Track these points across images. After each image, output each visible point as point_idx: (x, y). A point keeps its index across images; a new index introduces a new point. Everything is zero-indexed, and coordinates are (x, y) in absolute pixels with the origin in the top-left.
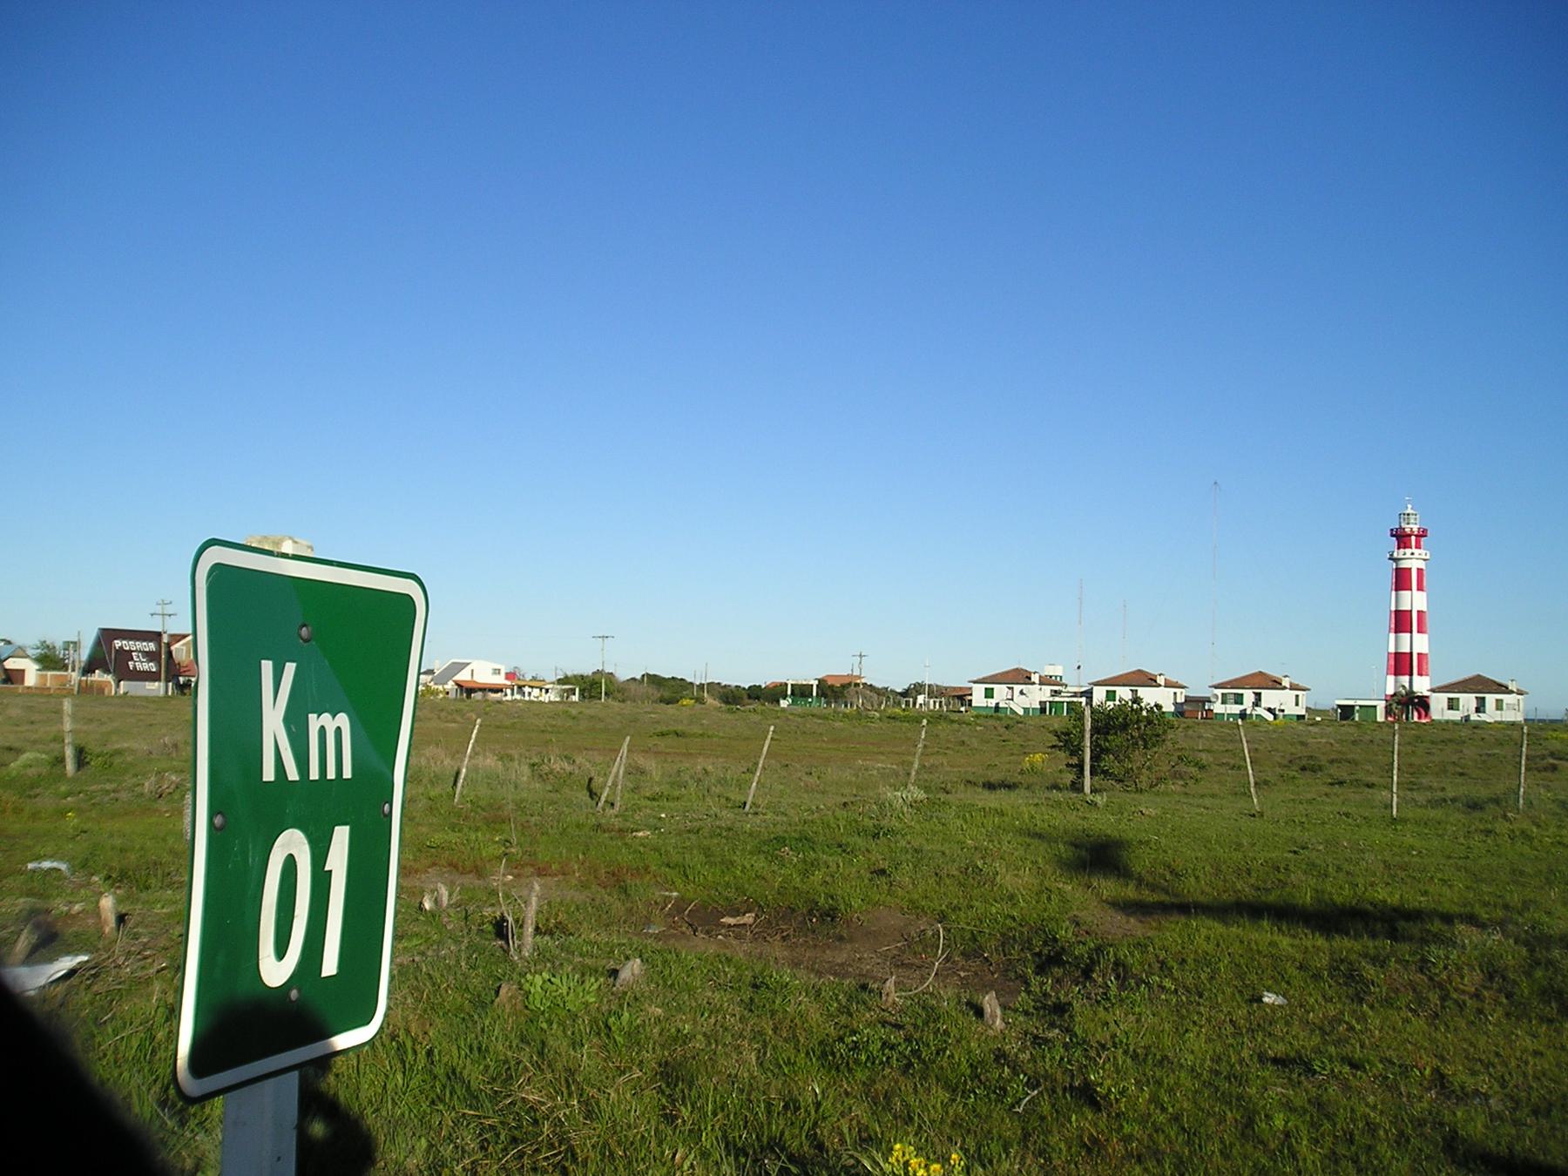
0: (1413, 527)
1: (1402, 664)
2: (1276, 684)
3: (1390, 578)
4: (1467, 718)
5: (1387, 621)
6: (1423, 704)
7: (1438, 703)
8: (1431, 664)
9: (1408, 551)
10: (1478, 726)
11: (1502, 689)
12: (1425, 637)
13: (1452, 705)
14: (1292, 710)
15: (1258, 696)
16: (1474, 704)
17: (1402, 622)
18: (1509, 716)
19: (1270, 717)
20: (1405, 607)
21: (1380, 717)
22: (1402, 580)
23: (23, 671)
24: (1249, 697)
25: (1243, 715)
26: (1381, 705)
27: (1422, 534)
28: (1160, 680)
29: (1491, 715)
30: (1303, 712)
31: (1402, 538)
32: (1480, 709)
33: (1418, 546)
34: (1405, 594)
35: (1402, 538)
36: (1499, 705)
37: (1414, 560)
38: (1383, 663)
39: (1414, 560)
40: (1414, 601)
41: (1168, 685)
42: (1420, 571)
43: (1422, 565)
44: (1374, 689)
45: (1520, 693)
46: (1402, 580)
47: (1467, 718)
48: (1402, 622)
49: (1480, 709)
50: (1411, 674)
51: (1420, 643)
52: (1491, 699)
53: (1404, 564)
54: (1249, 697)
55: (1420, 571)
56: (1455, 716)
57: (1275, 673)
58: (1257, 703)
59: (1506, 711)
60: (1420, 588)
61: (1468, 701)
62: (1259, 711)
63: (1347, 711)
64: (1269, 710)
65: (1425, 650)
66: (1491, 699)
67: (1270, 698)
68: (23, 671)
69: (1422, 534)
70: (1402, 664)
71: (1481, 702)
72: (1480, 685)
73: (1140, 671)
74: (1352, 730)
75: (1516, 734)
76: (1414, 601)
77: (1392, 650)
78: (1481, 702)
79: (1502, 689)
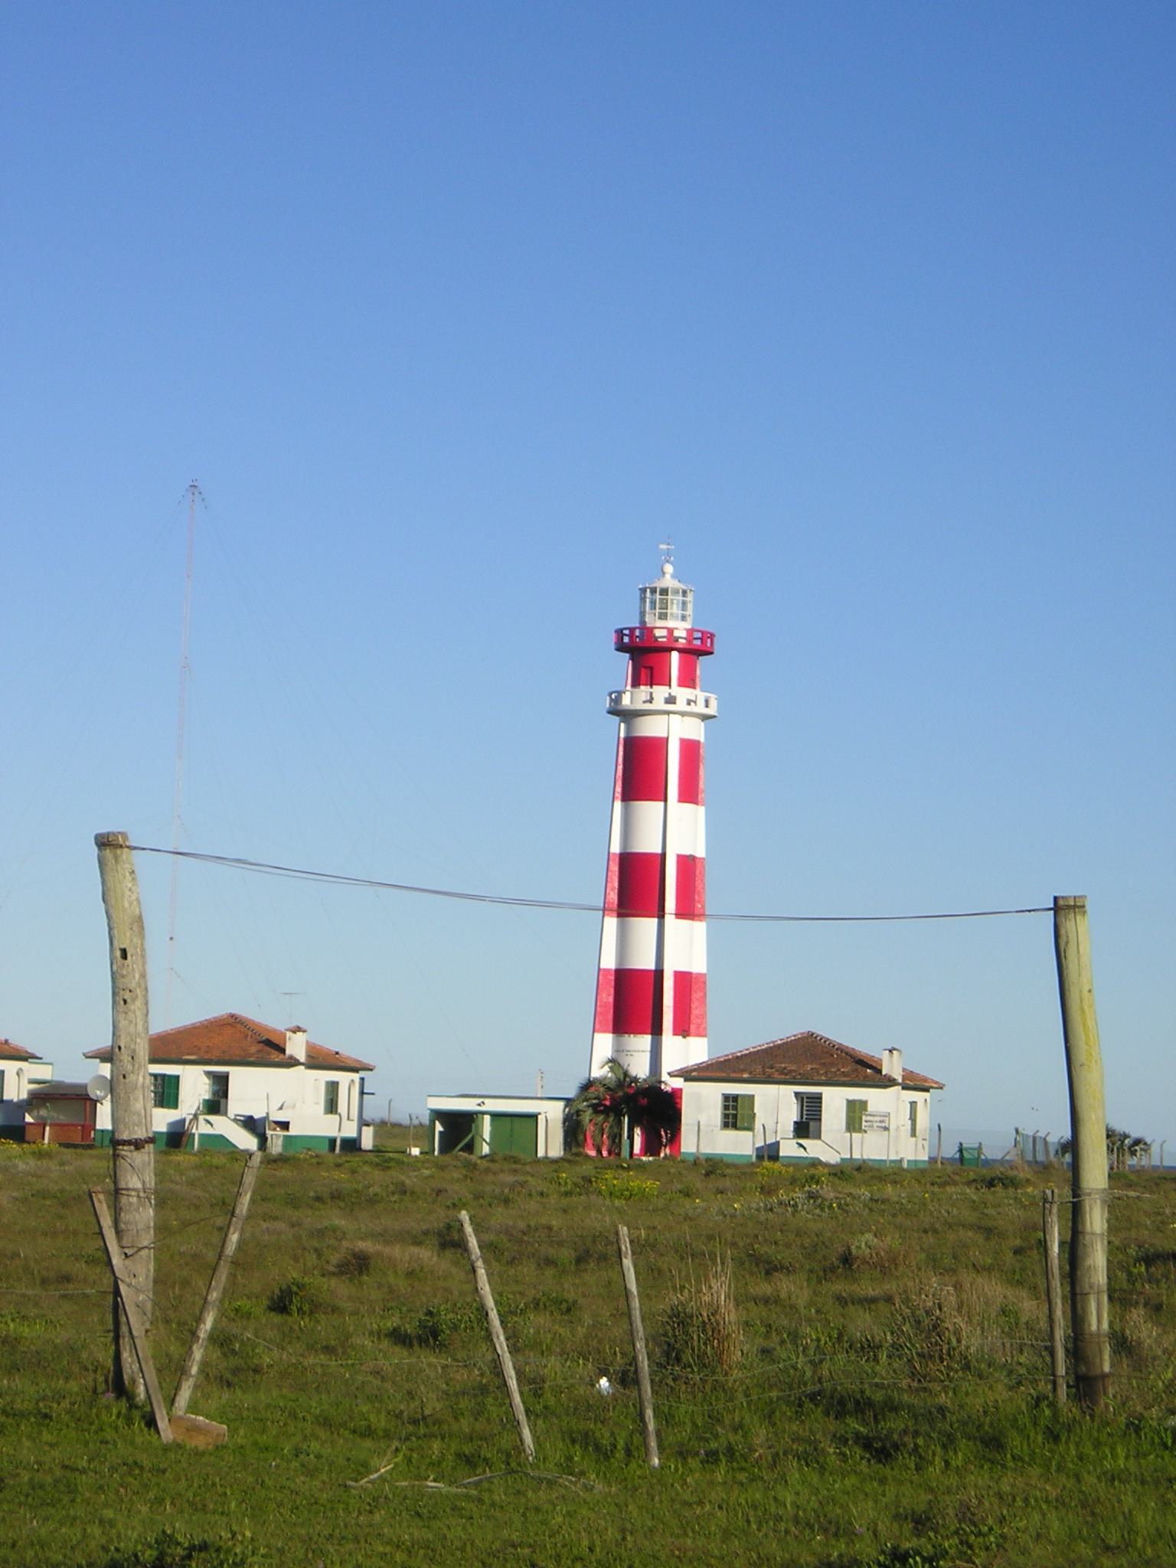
0: (676, 625)
1: (633, 1002)
2: (268, 1050)
3: (607, 765)
4: (770, 1152)
5: (599, 883)
6: (654, 1109)
7: (702, 1106)
8: (714, 1006)
9: (660, 692)
10: (809, 1172)
11: (863, 1071)
12: (699, 928)
13: (736, 1114)
14: (310, 1120)
15: (221, 1083)
16: (791, 1113)
17: (637, 886)
18: (871, 1148)
19: (247, 1141)
20: (648, 844)
21: (550, 1143)
22: (640, 772)
23: (178, 1077)
24: (195, 1084)
25: (177, 1137)
26: (552, 1113)
27: (697, 650)
28: (296, 1046)
29: (832, 1145)
30: (350, 1131)
31: (645, 656)
32: (807, 1126)
33: (688, 680)
34: (649, 811)
35: (645, 656)
36: (855, 1114)
37: (675, 717)
38: (585, 999)
39: (675, 717)
40: (675, 829)
41: (319, 1060)
42: (690, 749)
43: (695, 730)
44: (536, 1062)
45: (914, 1083)
46: (640, 772)
47: (770, 1152)
48: (637, 886)
49: (807, 1126)
50: (657, 1031)
51: (684, 946)
52: (835, 1100)
53: (650, 728)
54: (195, 1084)
55: (690, 749)
56: (739, 1145)
57: (268, 1016)
58: (215, 1105)
59: (893, 1131)
60: (690, 793)
61: (776, 1105)
62: (223, 1126)
63: (458, 1127)
64: (250, 1124)
65: (698, 965)
66: (835, 1100)
67: (254, 1089)
68: (178, 1077)
69: (697, 650)
70: (633, 1002)
71: (811, 1108)
72: (813, 1062)
73: (232, 1016)
74: (193, 1158)
75: (1008, 1210)
76: (675, 829)
77: (609, 962)
78: (811, 1108)
79: (863, 1071)
